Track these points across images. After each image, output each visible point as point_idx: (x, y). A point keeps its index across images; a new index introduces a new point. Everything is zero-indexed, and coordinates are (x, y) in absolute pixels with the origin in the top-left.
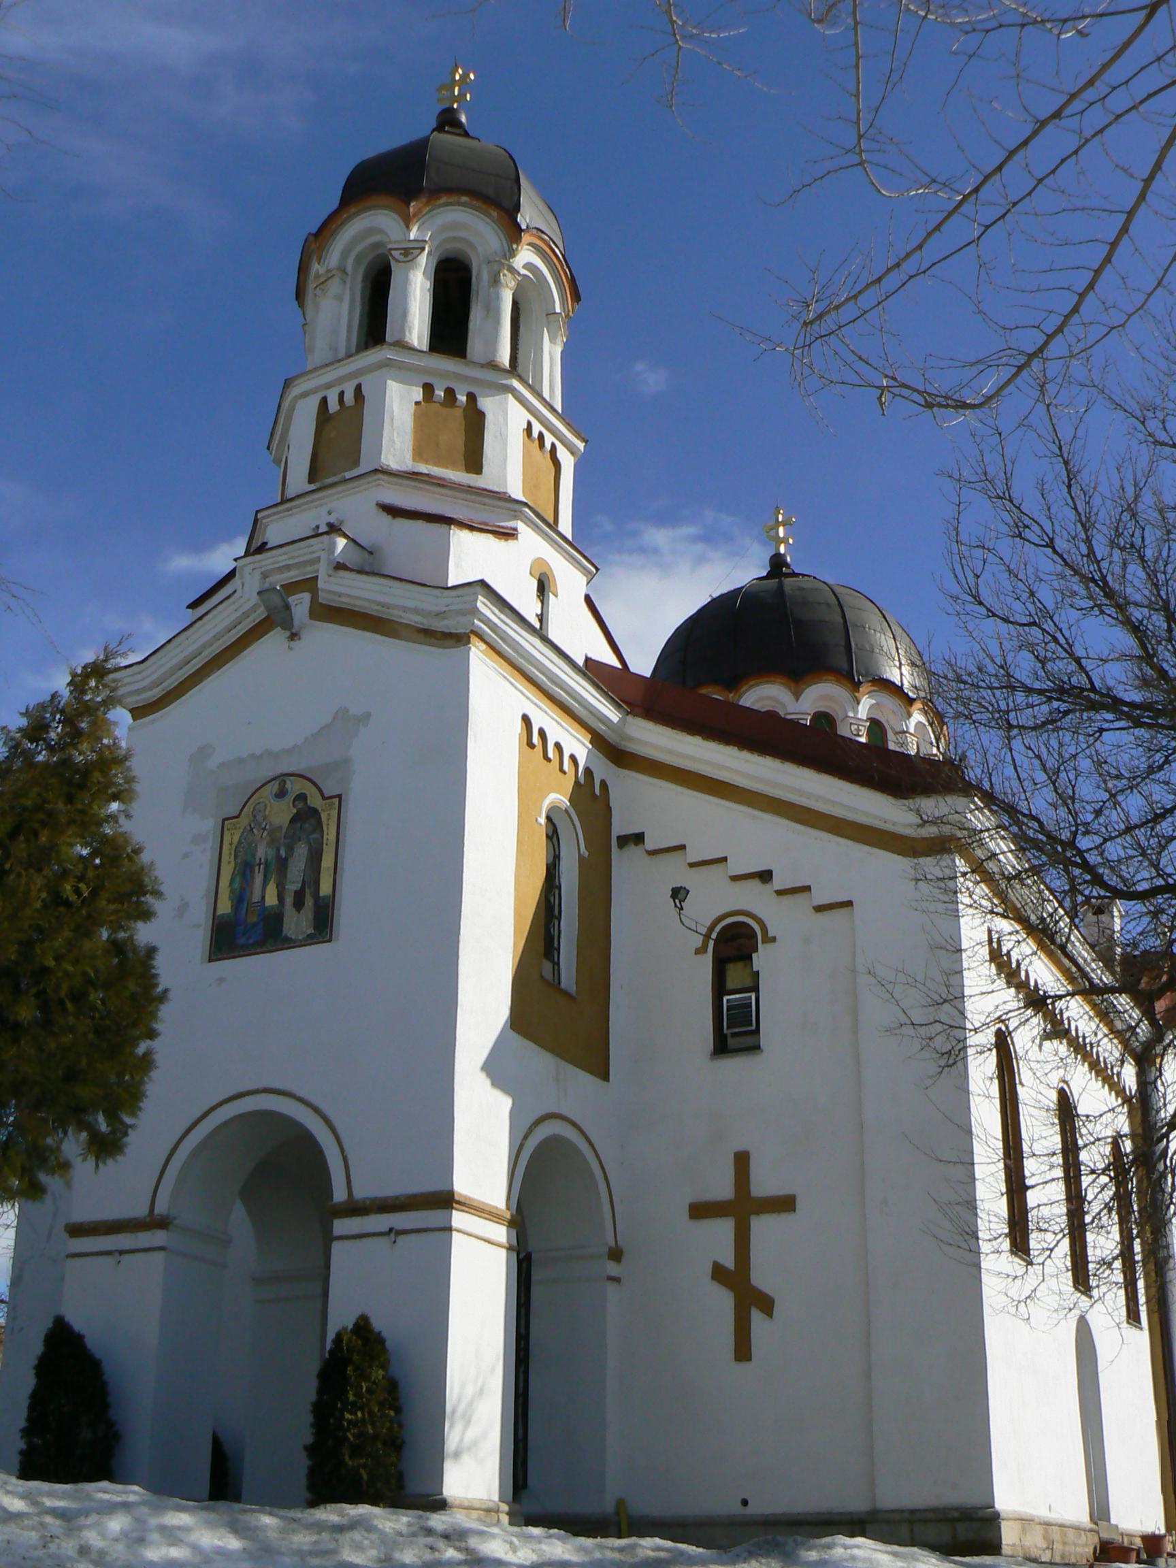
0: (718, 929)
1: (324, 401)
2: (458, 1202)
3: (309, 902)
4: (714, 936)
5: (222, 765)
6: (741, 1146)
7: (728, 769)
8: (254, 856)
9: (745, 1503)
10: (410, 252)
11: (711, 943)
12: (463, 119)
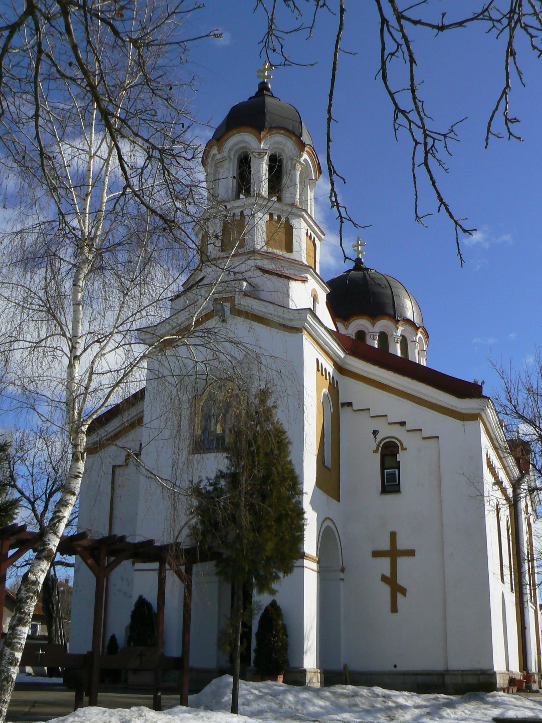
0: (383, 443)
2: (306, 556)
4: (381, 445)
7: (388, 380)
8: (211, 412)
9: (395, 666)
10: (260, 154)
11: (380, 449)
12: (270, 86)
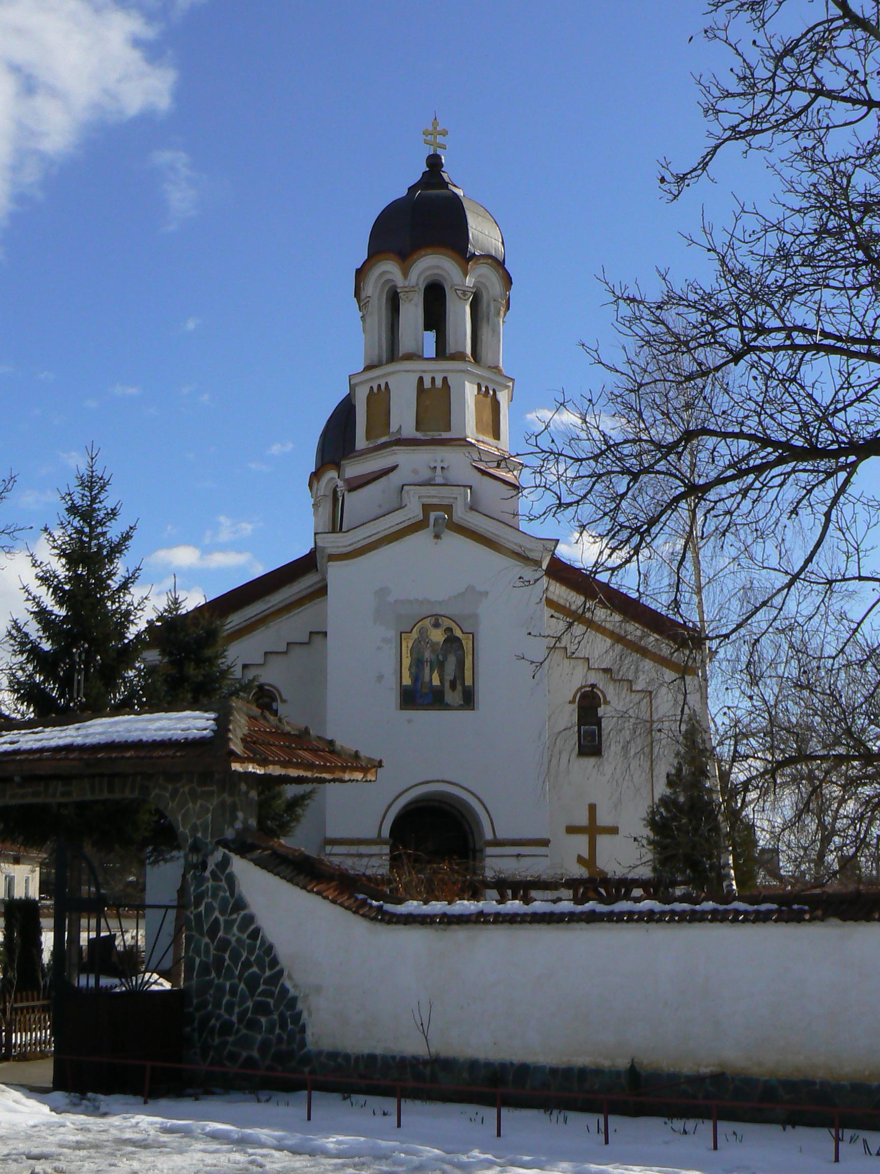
1: (421, 380)
3: (459, 687)
5: (396, 601)
6: (592, 801)
